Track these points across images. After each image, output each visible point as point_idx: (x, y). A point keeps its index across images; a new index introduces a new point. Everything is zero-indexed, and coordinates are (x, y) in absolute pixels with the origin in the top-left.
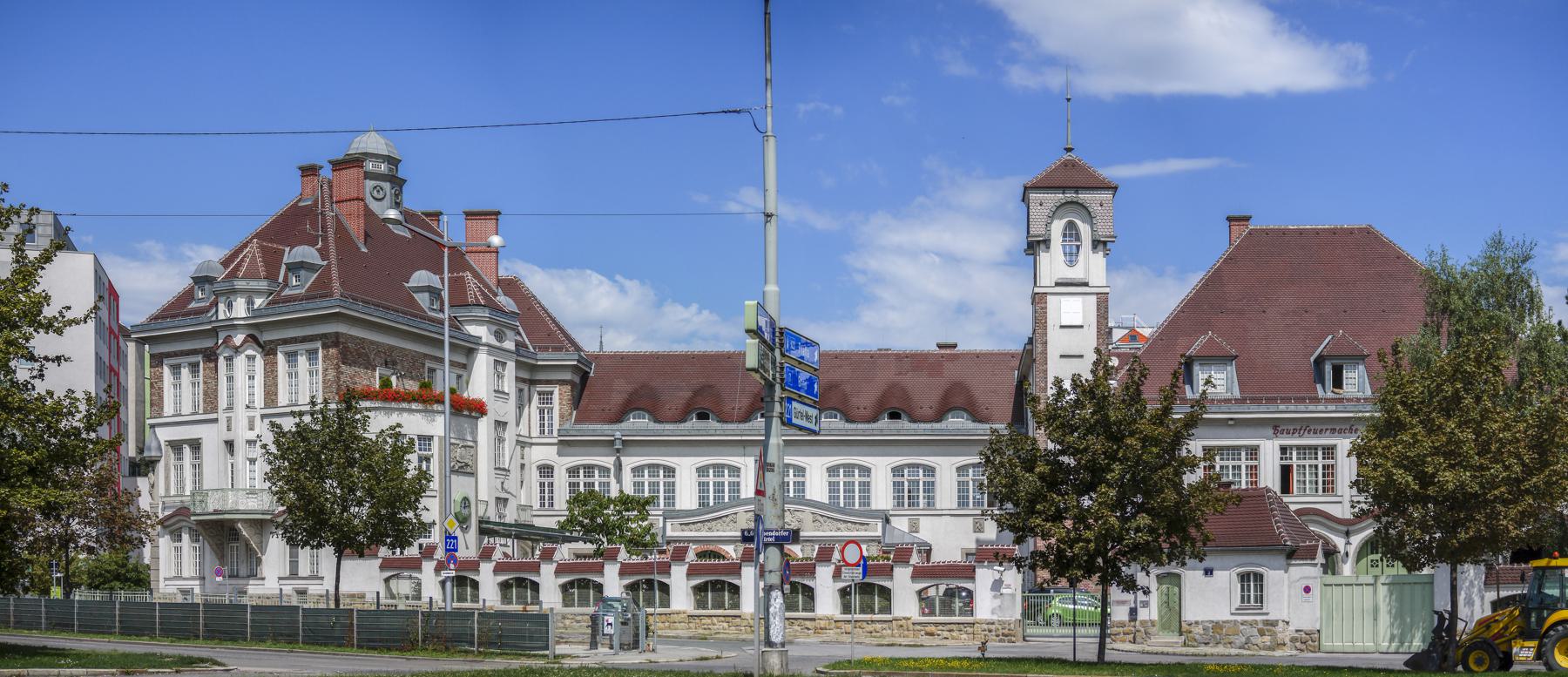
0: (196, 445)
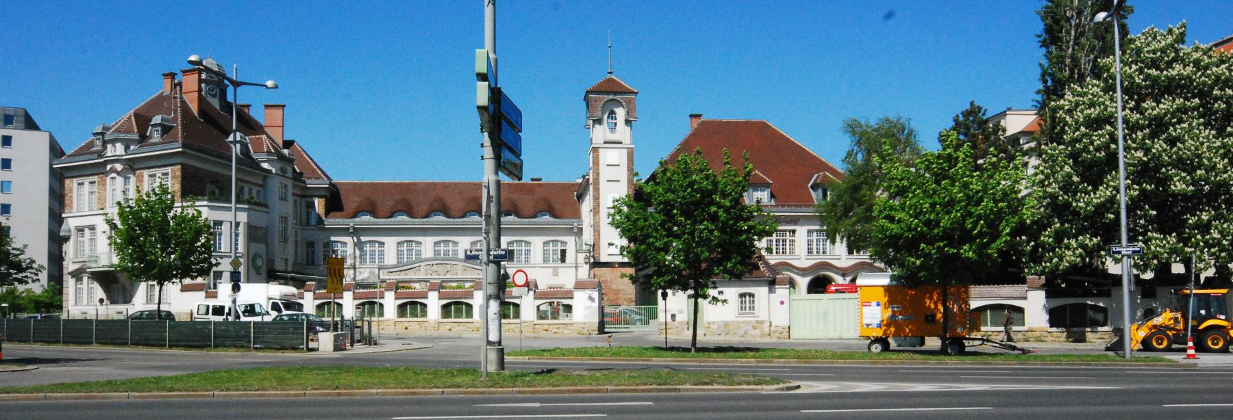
0: (92, 228)
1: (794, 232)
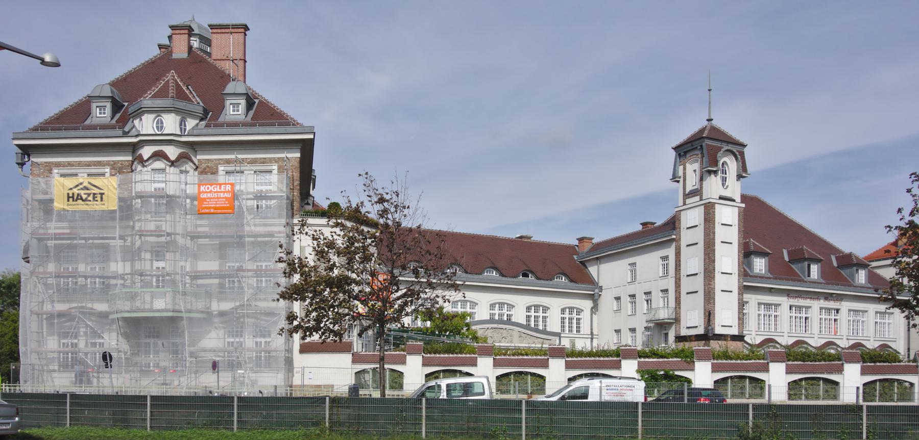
1: (838, 311)
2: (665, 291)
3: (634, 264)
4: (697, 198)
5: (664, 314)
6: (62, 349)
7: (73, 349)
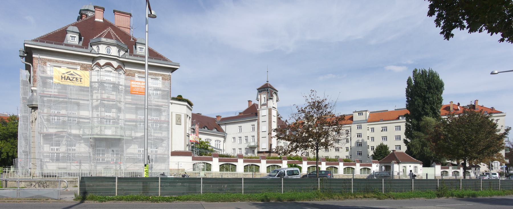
2: (253, 136)
3: (241, 127)
4: (266, 107)
5: (252, 144)
6: (51, 151)
7: (52, 152)
